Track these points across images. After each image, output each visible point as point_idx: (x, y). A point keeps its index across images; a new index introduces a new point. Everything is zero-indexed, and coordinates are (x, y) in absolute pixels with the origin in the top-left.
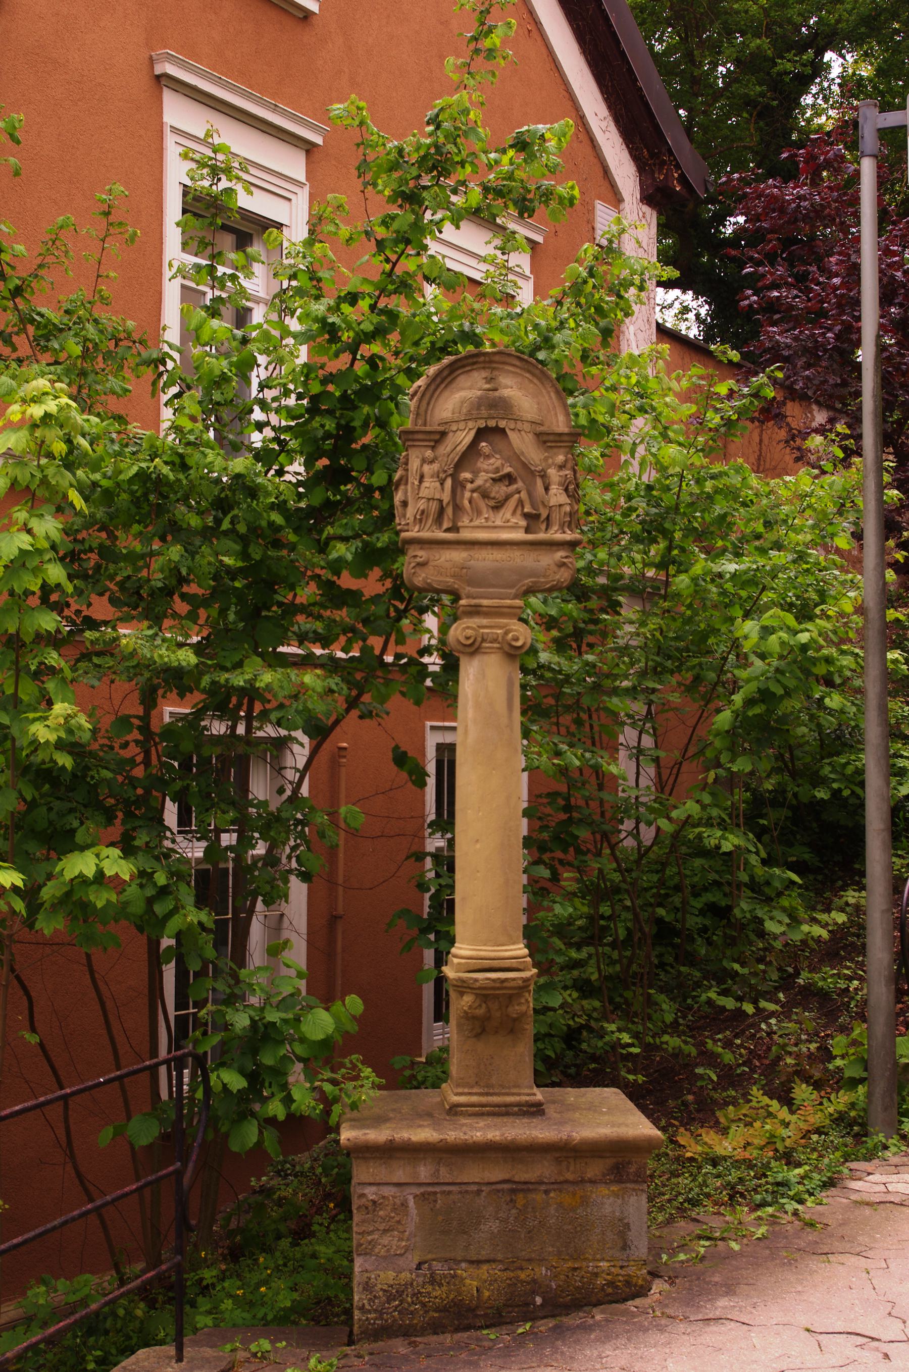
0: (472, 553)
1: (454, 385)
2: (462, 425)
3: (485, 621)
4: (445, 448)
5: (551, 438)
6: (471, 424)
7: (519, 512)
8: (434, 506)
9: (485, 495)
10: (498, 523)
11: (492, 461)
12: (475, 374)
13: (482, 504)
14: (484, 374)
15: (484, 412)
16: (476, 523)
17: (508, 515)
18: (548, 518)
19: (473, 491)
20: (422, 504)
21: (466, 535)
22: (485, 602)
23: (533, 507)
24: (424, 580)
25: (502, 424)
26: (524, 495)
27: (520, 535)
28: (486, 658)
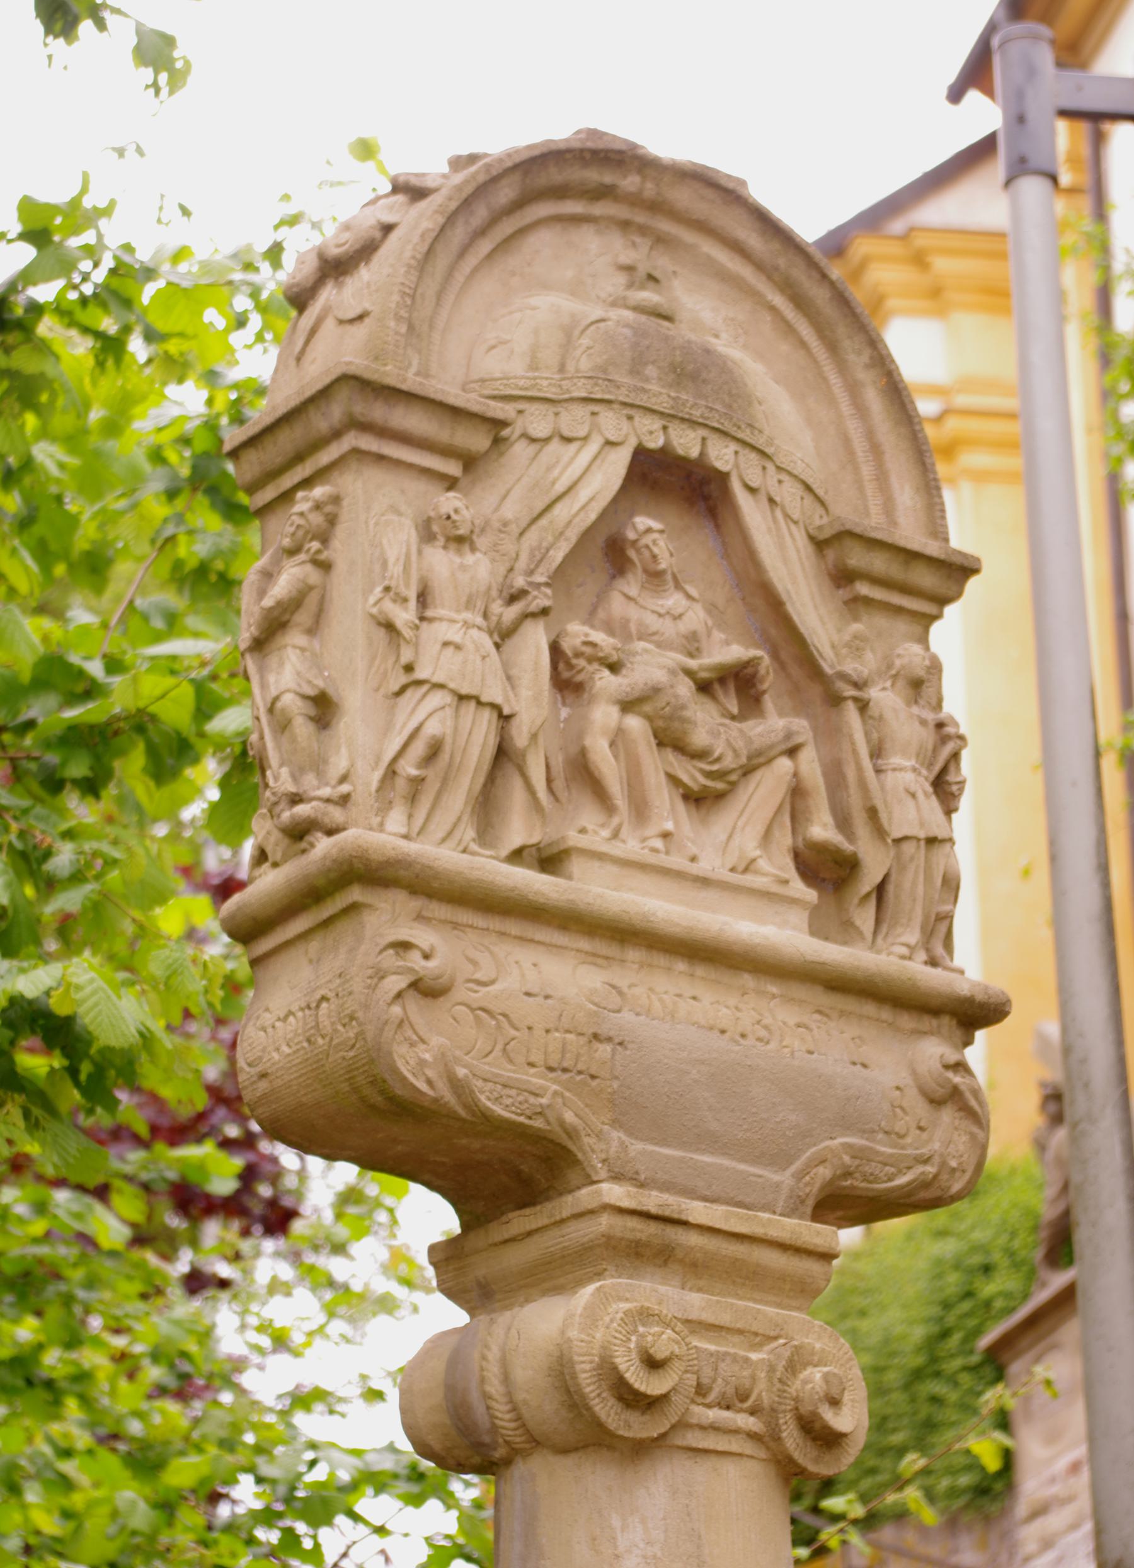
0: (623, 977)
1: (512, 261)
2: (574, 420)
3: (695, 1302)
4: (504, 495)
5: (878, 563)
6: (611, 423)
7: (784, 839)
8: (480, 736)
9: (669, 739)
10: (710, 864)
11: (673, 601)
12: (590, 240)
13: (655, 766)
14: (637, 253)
15: (660, 395)
16: (631, 846)
17: (748, 843)
18: (881, 889)
19: (627, 706)
20: (429, 714)
21: (591, 887)
22: (698, 1211)
23: (843, 823)
24: (444, 1062)
25: (722, 456)
26: (810, 763)
27: (786, 933)
28: (700, 1472)
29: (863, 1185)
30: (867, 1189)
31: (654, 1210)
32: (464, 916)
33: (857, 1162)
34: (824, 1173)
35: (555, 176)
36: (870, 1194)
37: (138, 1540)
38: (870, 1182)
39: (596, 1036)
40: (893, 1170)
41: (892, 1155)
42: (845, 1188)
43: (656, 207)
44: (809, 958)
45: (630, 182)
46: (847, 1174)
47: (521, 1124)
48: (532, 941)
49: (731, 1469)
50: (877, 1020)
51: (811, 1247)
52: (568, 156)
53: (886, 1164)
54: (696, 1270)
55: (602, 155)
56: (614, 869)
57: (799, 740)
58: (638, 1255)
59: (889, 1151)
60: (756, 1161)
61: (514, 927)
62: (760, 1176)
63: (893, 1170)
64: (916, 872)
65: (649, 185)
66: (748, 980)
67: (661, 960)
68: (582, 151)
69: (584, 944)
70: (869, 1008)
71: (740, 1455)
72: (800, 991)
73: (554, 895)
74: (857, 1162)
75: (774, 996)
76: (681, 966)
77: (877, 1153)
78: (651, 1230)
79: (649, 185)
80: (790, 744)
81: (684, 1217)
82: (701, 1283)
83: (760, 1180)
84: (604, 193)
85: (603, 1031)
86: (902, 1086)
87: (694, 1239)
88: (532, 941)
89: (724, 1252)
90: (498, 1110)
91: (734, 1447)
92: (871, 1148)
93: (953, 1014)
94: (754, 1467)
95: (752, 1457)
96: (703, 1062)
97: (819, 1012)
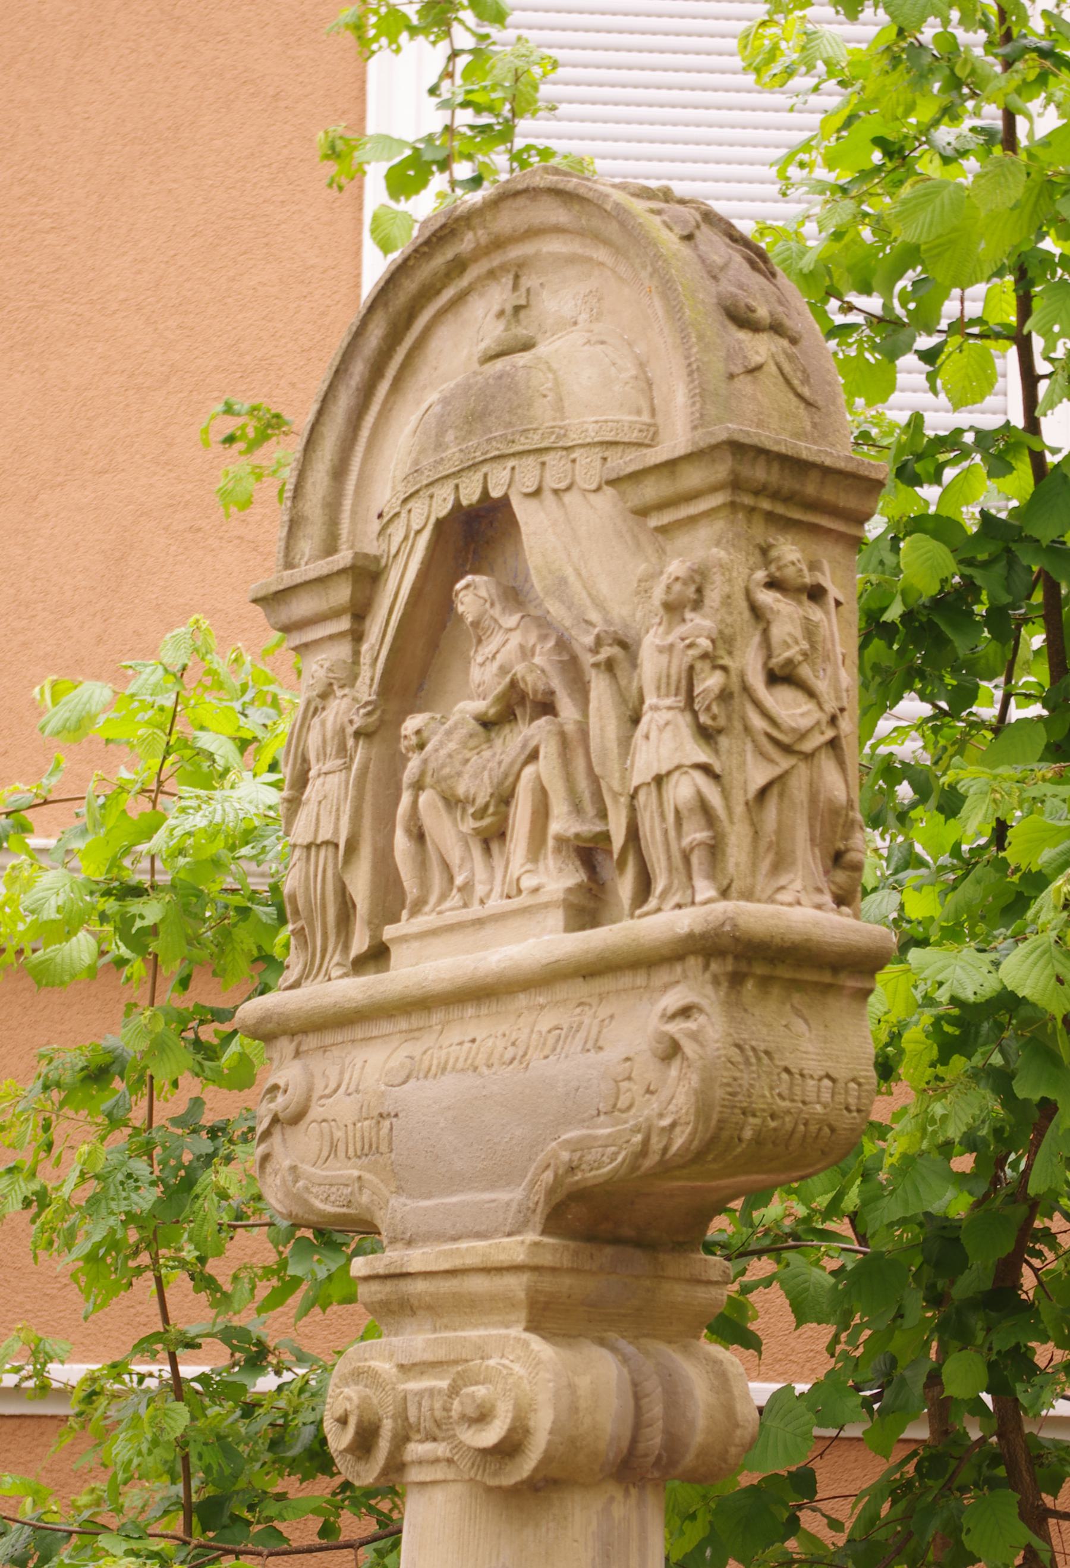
29: (593, 1173)
30: (595, 1177)
31: (381, 1271)
32: (329, 1038)
33: (578, 1154)
34: (548, 1176)
35: (410, 286)
36: (601, 1180)
37: (724, 1466)
38: (598, 1168)
39: (381, 1115)
40: (613, 1149)
41: (610, 1135)
42: (577, 1182)
43: (498, 244)
44: (544, 962)
45: (466, 243)
46: (572, 1169)
47: (344, 1214)
48: (371, 1038)
49: (439, 1495)
50: (633, 989)
51: (499, 1265)
52: (411, 263)
53: (606, 1146)
54: (434, 1310)
55: (434, 239)
56: (415, 945)
57: (533, 744)
58: (391, 1312)
59: (609, 1130)
60: (492, 1187)
61: (359, 1032)
62: (493, 1201)
63: (613, 1149)
64: (652, 818)
65: (480, 232)
66: (522, 1000)
67: (455, 1013)
68: (416, 251)
69: (403, 1024)
70: (626, 980)
71: (445, 1481)
72: (562, 991)
73: (360, 996)
74: (578, 1154)
75: (542, 1007)
76: (470, 1011)
77: (596, 1138)
78: (388, 1287)
79: (480, 232)
80: (527, 752)
81: (404, 1270)
82: (445, 1320)
83: (493, 1205)
84: (459, 266)
85: (385, 1111)
86: (631, 1055)
87: (420, 1286)
88: (371, 1038)
89: (442, 1290)
90: (330, 1209)
91: (439, 1476)
92: (589, 1136)
93: (695, 953)
94: (457, 1489)
95: (454, 1481)
96: (449, 1108)
97: (580, 1004)
